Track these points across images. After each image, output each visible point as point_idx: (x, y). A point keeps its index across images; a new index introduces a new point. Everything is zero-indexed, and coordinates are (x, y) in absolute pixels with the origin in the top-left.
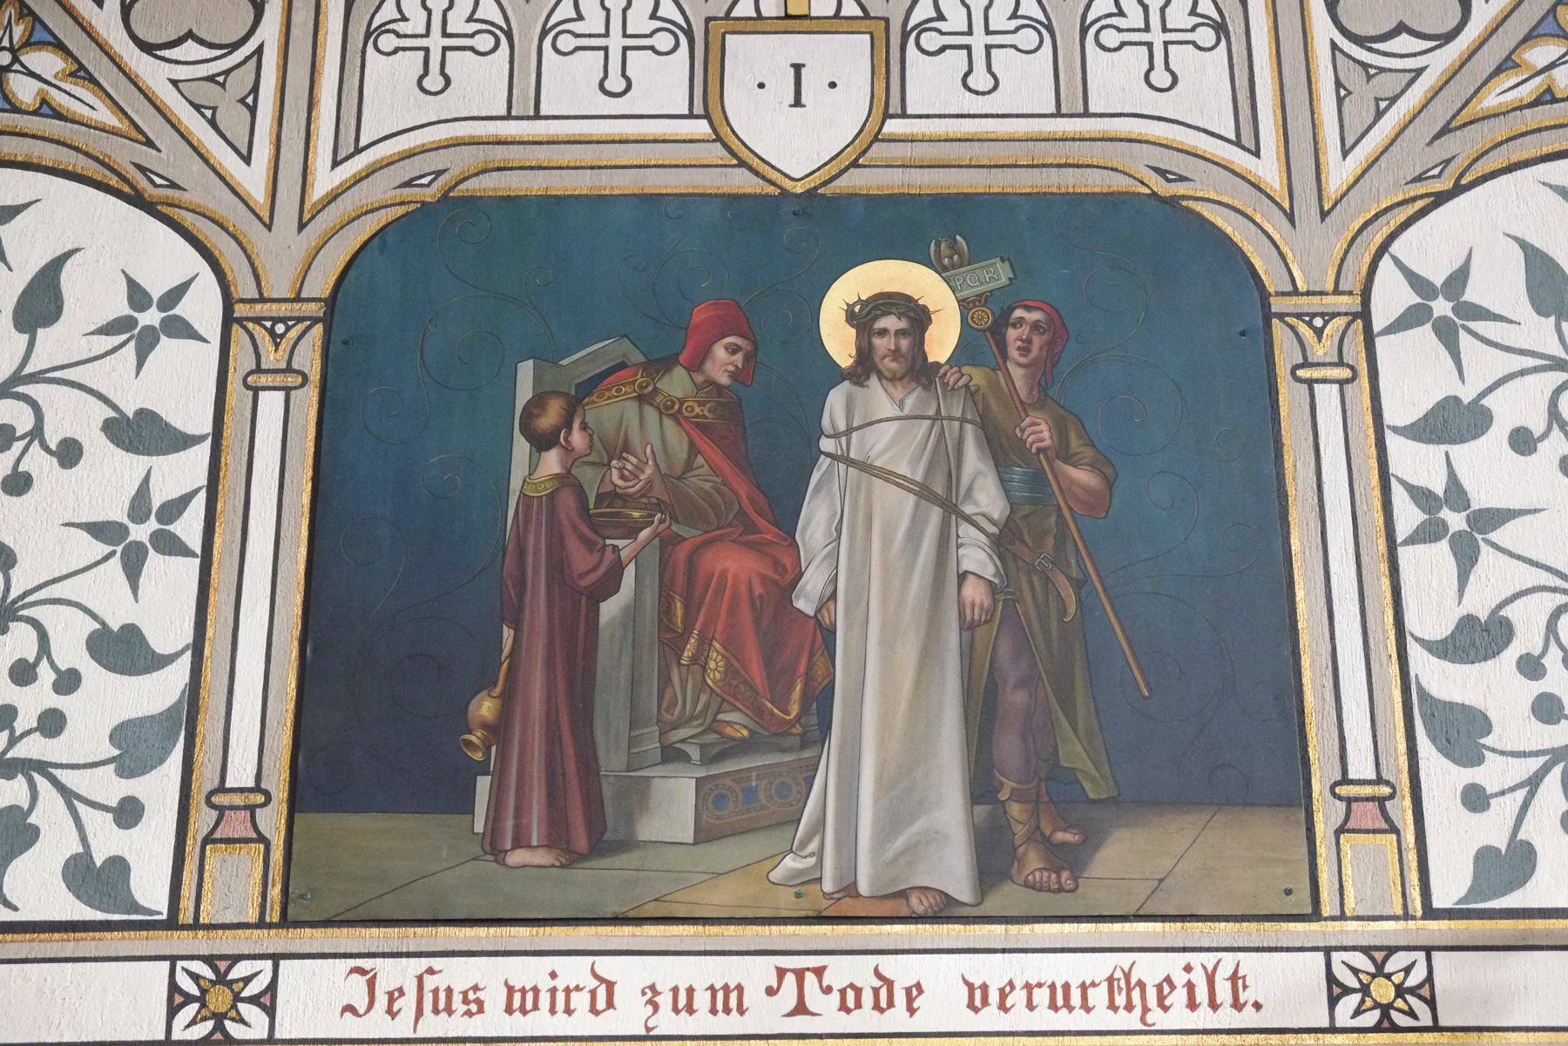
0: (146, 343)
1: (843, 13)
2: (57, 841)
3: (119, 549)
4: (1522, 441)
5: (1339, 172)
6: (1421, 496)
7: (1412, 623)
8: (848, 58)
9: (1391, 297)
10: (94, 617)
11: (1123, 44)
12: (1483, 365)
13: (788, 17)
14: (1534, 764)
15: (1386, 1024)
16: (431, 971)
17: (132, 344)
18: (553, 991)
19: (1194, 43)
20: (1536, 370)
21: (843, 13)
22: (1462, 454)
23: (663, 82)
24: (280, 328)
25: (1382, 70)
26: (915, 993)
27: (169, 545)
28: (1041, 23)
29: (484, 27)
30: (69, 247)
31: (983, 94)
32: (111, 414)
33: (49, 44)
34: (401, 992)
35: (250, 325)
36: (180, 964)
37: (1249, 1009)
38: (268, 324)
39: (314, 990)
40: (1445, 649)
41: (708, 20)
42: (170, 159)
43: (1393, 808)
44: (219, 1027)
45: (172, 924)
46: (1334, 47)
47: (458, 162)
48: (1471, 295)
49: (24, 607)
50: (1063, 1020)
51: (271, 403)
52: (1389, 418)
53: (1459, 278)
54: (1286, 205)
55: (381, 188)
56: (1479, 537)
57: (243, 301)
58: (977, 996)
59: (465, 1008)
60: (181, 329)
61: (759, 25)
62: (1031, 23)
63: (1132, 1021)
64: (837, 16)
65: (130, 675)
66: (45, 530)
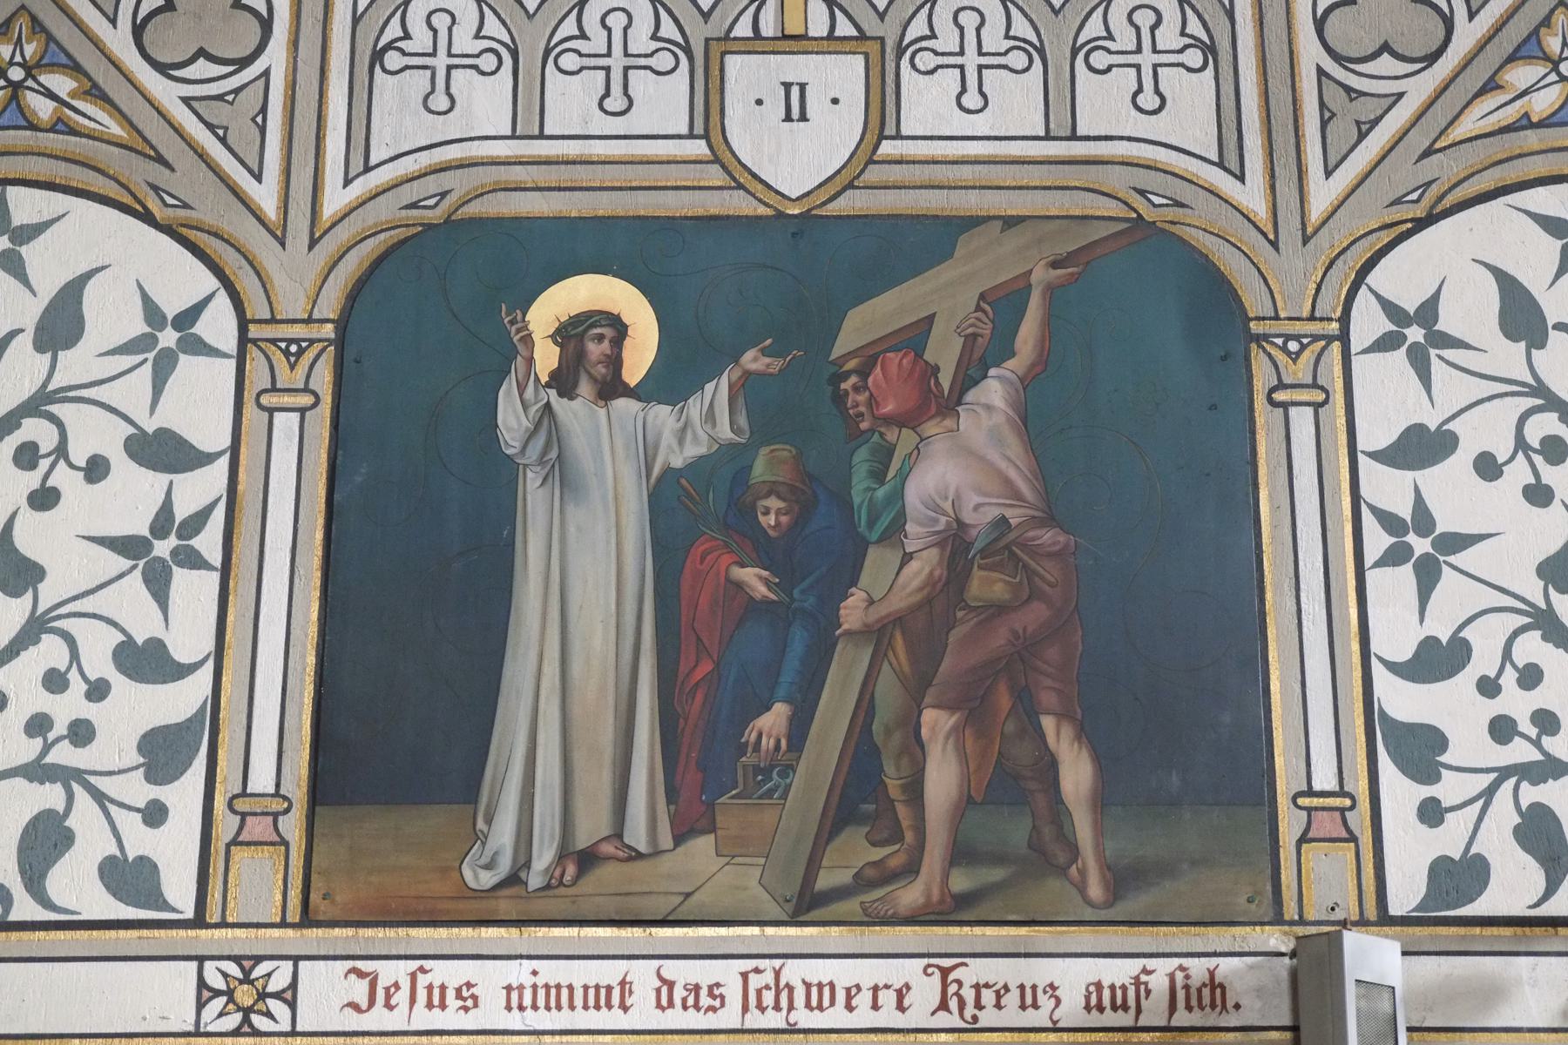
0: (164, 368)
1: (838, 33)
3: (141, 563)
4: (1488, 467)
5: (1323, 193)
6: (1389, 522)
8: (840, 77)
9: (1368, 322)
10: (123, 631)
11: (407, 67)
12: (1452, 388)
13: (785, 37)
14: (1486, 780)
16: (422, 970)
18: (535, 987)
20: (1513, 394)
21: (838, 33)
23: (663, 102)
25: (237, 91)
26: (854, 991)
27: (194, 561)
28: (1031, 44)
29: (1017, 43)
32: (131, 430)
33: (64, 66)
34: (397, 986)
36: (208, 965)
38: (283, 345)
39: (326, 994)
40: (1392, 667)
41: (707, 40)
42: (187, 180)
43: (1354, 825)
45: (199, 921)
46: (1321, 72)
47: (459, 183)
48: (171, 310)
49: (59, 617)
50: (438, 1020)
51: (286, 423)
52: (1362, 444)
53: (153, 313)
55: (385, 210)
57: (1258, 319)
58: (468, 997)
59: (461, 1003)
60: (199, 347)
61: (758, 46)
62: (1197, 43)
63: (774, 1020)
64: (831, 36)
66: (60, 546)
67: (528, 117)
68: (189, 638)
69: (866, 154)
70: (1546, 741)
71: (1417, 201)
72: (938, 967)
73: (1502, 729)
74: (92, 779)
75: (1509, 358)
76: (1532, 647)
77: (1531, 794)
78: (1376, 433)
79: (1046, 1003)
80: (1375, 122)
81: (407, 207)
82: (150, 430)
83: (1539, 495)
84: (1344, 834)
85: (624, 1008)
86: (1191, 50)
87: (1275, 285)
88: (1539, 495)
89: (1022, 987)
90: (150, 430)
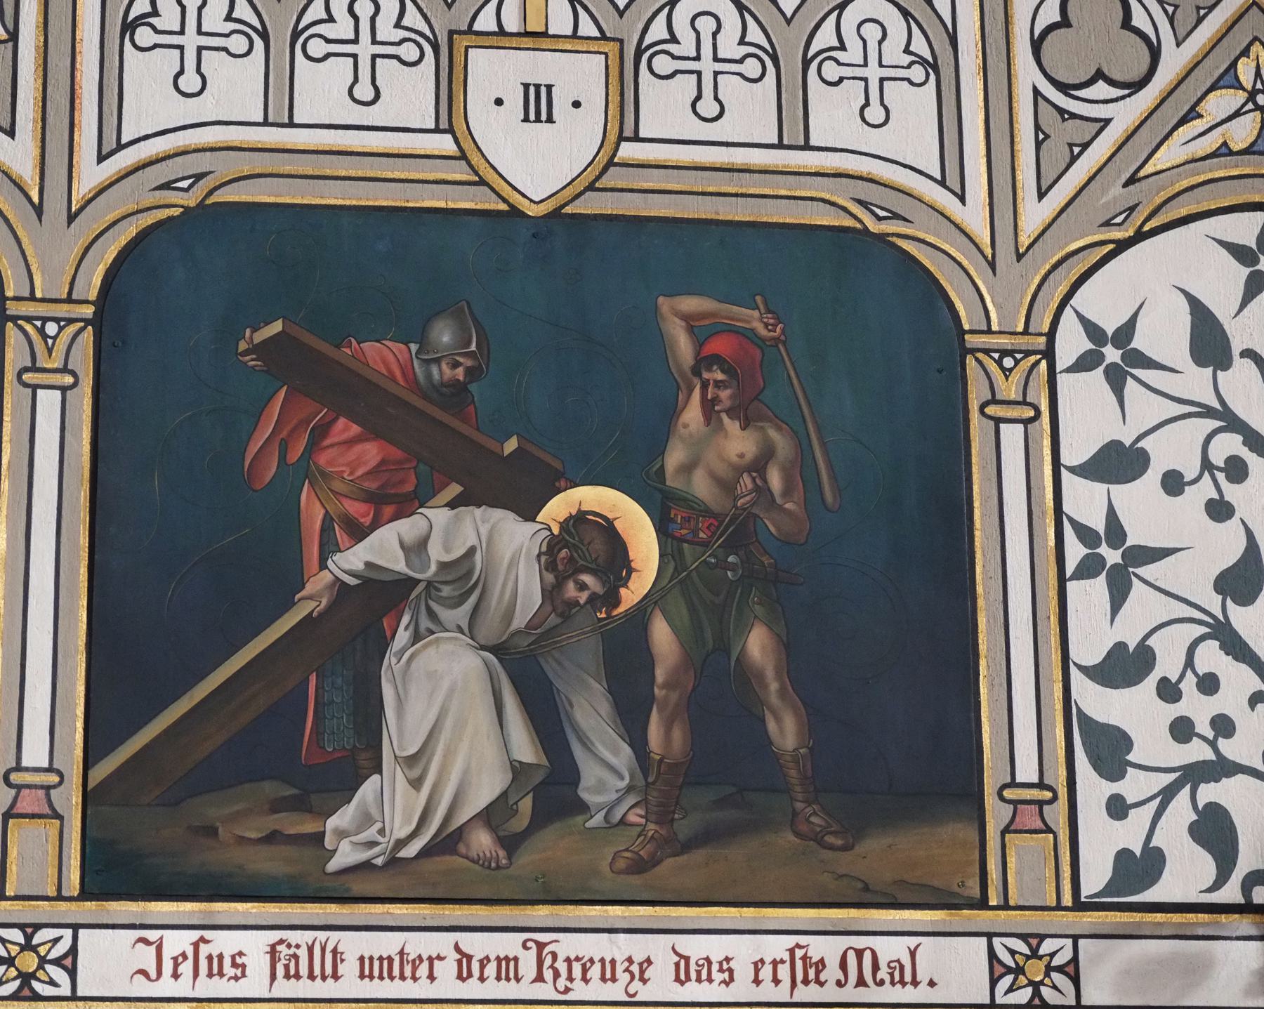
5: (1034, 214)
6: (1086, 535)
8: (580, 77)
9: (1071, 343)
12: (1144, 408)
13: (528, 34)
19: (908, 80)
22: (1120, 493)
23: (410, 94)
24: (1009, 362)
29: (413, 36)
35: (980, 355)
37: (923, 986)
39: (110, 954)
40: (1080, 668)
43: (1047, 810)
44: (1037, 993)
46: (1036, 92)
52: (1067, 458)
54: (988, 252)
57: (972, 332)
58: (683, 971)
62: (923, 61)
64: (575, 36)
70: (1222, 743)
71: (880, 219)
72: (536, 942)
73: (1182, 730)
75: (1196, 382)
76: (1211, 657)
77: (1208, 793)
80: (1085, 146)
84: (47, 811)
85: (336, 976)
87: (986, 303)
88: (1219, 510)
89: (602, 961)
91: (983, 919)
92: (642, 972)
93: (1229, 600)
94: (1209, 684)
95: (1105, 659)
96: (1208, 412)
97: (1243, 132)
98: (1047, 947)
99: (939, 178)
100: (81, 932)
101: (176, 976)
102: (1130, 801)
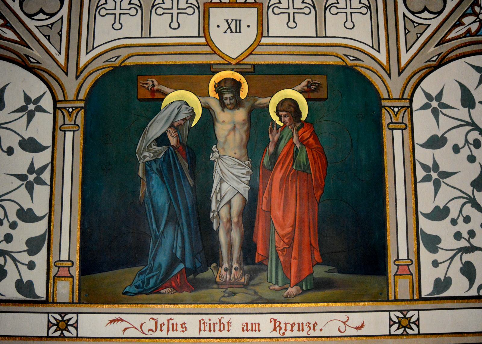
0: (30, 116)
2: (12, 276)
4: (456, 149)
5: (405, 58)
6: (425, 167)
7: (420, 209)
8: (249, 16)
9: (419, 100)
11: (107, 14)
12: (445, 123)
15: (75, 325)
16: (171, 319)
17: (26, 116)
18: (210, 324)
22: (437, 152)
23: (190, 25)
26: (293, 325)
27: (43, 183)
30: (8, 83)
31: (293, 28)
32: (21, 139)
35: (386, 108)
36: (50, 314)
39: (93, 322)
41: (204, 3)
42: (36, 53)
46: (405, 16)
48: (33, 98)
50: (172, 334)
55: (100, 62)
56: (441, 180)
58: (256, 327)
59: (182, 329)
60: (40, 109)
63: (304, 334)
65: (30, 223)
67: (146, 29)
68: (41, 209)
69: (257, 43)
70: (471, 240)
74: (13, 254)
75: (463, 113)
76: (469, 210)
77: (467, 257)
78: (421, 137)
79: (306, 329)
81: (427, 62)
82: (26, 138)
83: (472, 159)
85: (228, 330)
86: (363, 8)
87: (391, 87)
89: (299, 324)
90: (26, 138)
91: (48, 309)
92: (314, 327)
93: (475, 190)
94: (467, 220)
95: (432, 211)
96: (468, 124)
97: (474, 27)
98: (67, 317)
99: (371, 46)
100: (420, 312)
101: (161, 330)
102: (439, 262)
